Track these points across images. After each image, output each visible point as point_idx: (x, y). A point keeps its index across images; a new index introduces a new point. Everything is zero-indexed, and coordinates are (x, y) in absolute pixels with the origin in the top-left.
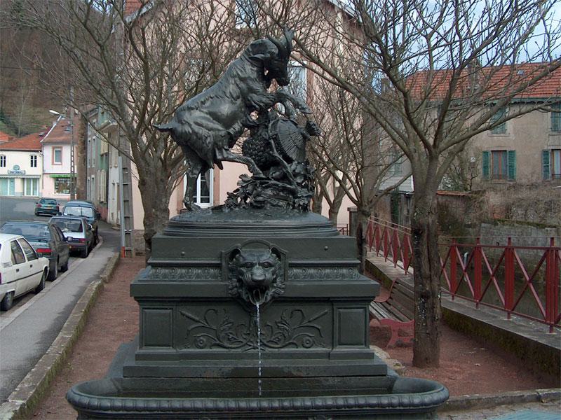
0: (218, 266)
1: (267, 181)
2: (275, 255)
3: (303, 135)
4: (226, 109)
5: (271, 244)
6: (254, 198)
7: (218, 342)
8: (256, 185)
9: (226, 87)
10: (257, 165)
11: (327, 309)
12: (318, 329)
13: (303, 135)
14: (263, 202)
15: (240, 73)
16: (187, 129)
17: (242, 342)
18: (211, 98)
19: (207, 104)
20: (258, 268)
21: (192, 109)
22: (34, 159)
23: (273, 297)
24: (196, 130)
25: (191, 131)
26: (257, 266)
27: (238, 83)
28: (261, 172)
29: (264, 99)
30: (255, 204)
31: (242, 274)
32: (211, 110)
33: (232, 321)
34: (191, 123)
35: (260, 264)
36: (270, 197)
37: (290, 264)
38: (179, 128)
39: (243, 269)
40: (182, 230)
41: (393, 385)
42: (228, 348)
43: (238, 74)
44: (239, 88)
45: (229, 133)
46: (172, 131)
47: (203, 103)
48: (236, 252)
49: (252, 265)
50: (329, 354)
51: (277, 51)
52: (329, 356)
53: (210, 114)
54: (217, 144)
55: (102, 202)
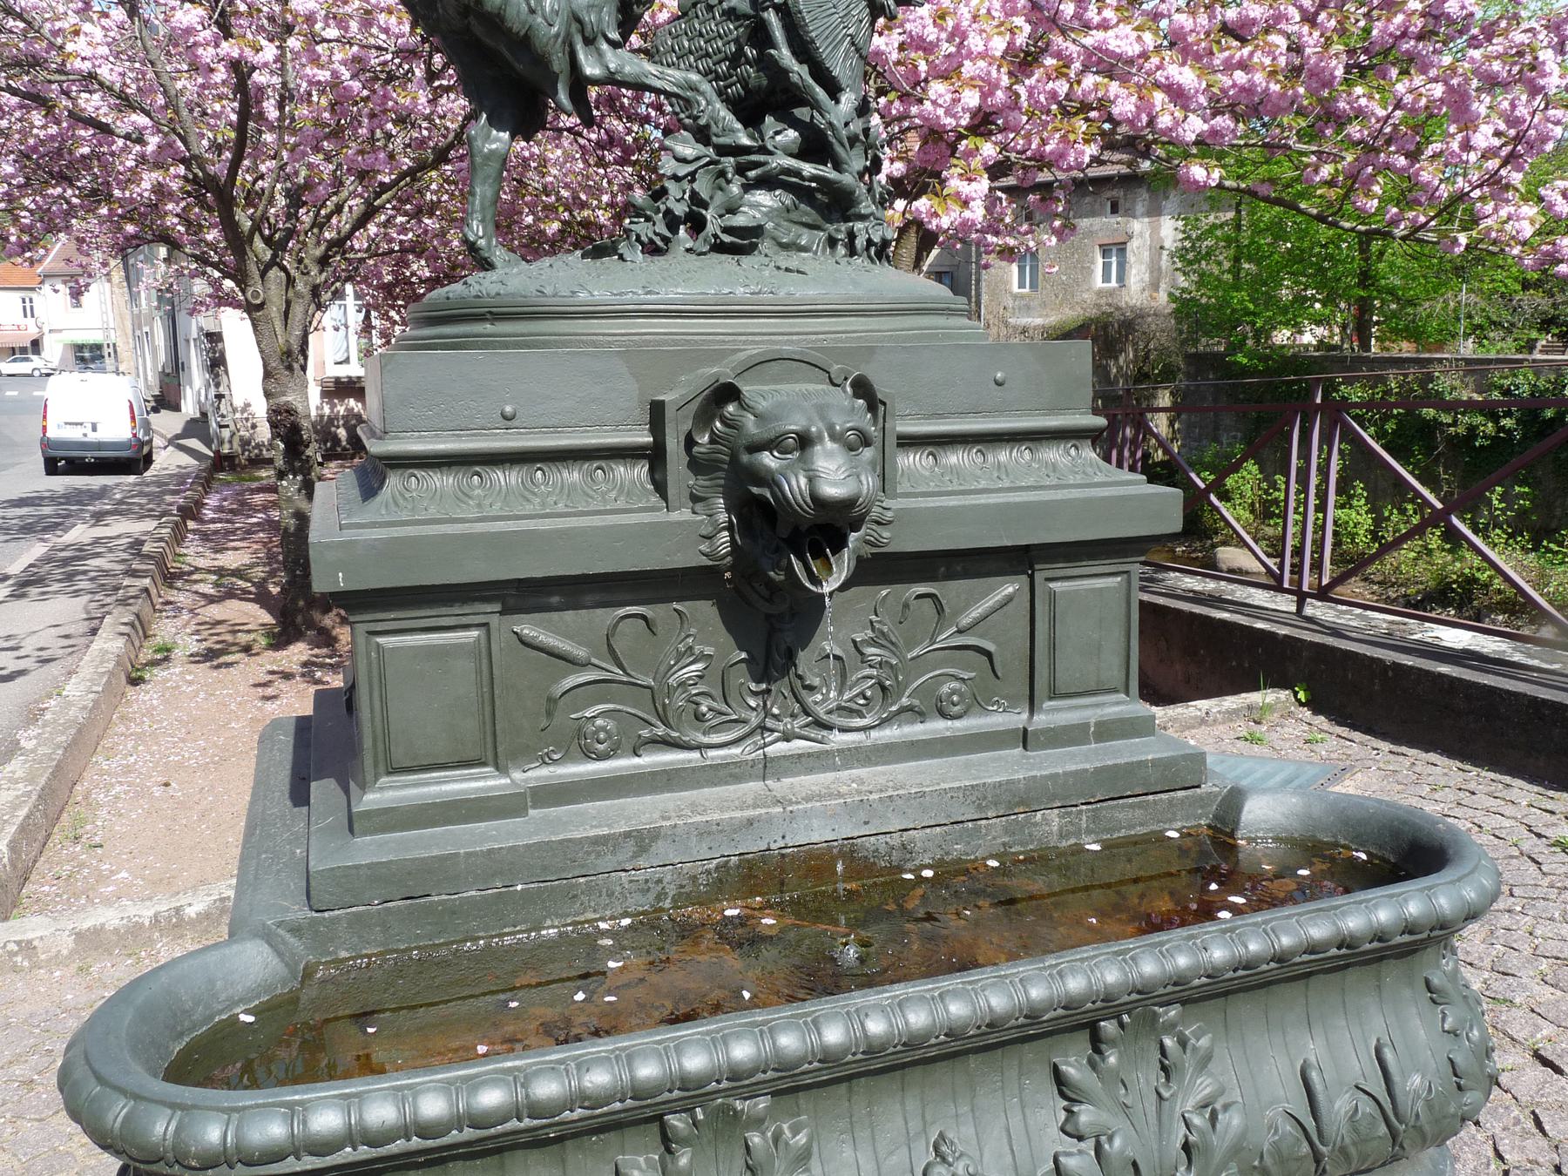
1: (762, 158)
7: (661, 731)
8: (722, 174)
11: (1009, 587)
12: (989, 655)
14: (757, 231)
17: (745, 722)
20: (829, 455)
22: (28, 304)
26: (829, 444)
28: (739, 126)
30: (727, 239)
33: (709, 651)
39: (769, 460)
40: (488, 327)
41: (1236, 822)
42: (699, 747)
48: (726, 393)
49: (805, 441)
50: (1025, 730)
52: (1025, 738)
54: (579, 20)
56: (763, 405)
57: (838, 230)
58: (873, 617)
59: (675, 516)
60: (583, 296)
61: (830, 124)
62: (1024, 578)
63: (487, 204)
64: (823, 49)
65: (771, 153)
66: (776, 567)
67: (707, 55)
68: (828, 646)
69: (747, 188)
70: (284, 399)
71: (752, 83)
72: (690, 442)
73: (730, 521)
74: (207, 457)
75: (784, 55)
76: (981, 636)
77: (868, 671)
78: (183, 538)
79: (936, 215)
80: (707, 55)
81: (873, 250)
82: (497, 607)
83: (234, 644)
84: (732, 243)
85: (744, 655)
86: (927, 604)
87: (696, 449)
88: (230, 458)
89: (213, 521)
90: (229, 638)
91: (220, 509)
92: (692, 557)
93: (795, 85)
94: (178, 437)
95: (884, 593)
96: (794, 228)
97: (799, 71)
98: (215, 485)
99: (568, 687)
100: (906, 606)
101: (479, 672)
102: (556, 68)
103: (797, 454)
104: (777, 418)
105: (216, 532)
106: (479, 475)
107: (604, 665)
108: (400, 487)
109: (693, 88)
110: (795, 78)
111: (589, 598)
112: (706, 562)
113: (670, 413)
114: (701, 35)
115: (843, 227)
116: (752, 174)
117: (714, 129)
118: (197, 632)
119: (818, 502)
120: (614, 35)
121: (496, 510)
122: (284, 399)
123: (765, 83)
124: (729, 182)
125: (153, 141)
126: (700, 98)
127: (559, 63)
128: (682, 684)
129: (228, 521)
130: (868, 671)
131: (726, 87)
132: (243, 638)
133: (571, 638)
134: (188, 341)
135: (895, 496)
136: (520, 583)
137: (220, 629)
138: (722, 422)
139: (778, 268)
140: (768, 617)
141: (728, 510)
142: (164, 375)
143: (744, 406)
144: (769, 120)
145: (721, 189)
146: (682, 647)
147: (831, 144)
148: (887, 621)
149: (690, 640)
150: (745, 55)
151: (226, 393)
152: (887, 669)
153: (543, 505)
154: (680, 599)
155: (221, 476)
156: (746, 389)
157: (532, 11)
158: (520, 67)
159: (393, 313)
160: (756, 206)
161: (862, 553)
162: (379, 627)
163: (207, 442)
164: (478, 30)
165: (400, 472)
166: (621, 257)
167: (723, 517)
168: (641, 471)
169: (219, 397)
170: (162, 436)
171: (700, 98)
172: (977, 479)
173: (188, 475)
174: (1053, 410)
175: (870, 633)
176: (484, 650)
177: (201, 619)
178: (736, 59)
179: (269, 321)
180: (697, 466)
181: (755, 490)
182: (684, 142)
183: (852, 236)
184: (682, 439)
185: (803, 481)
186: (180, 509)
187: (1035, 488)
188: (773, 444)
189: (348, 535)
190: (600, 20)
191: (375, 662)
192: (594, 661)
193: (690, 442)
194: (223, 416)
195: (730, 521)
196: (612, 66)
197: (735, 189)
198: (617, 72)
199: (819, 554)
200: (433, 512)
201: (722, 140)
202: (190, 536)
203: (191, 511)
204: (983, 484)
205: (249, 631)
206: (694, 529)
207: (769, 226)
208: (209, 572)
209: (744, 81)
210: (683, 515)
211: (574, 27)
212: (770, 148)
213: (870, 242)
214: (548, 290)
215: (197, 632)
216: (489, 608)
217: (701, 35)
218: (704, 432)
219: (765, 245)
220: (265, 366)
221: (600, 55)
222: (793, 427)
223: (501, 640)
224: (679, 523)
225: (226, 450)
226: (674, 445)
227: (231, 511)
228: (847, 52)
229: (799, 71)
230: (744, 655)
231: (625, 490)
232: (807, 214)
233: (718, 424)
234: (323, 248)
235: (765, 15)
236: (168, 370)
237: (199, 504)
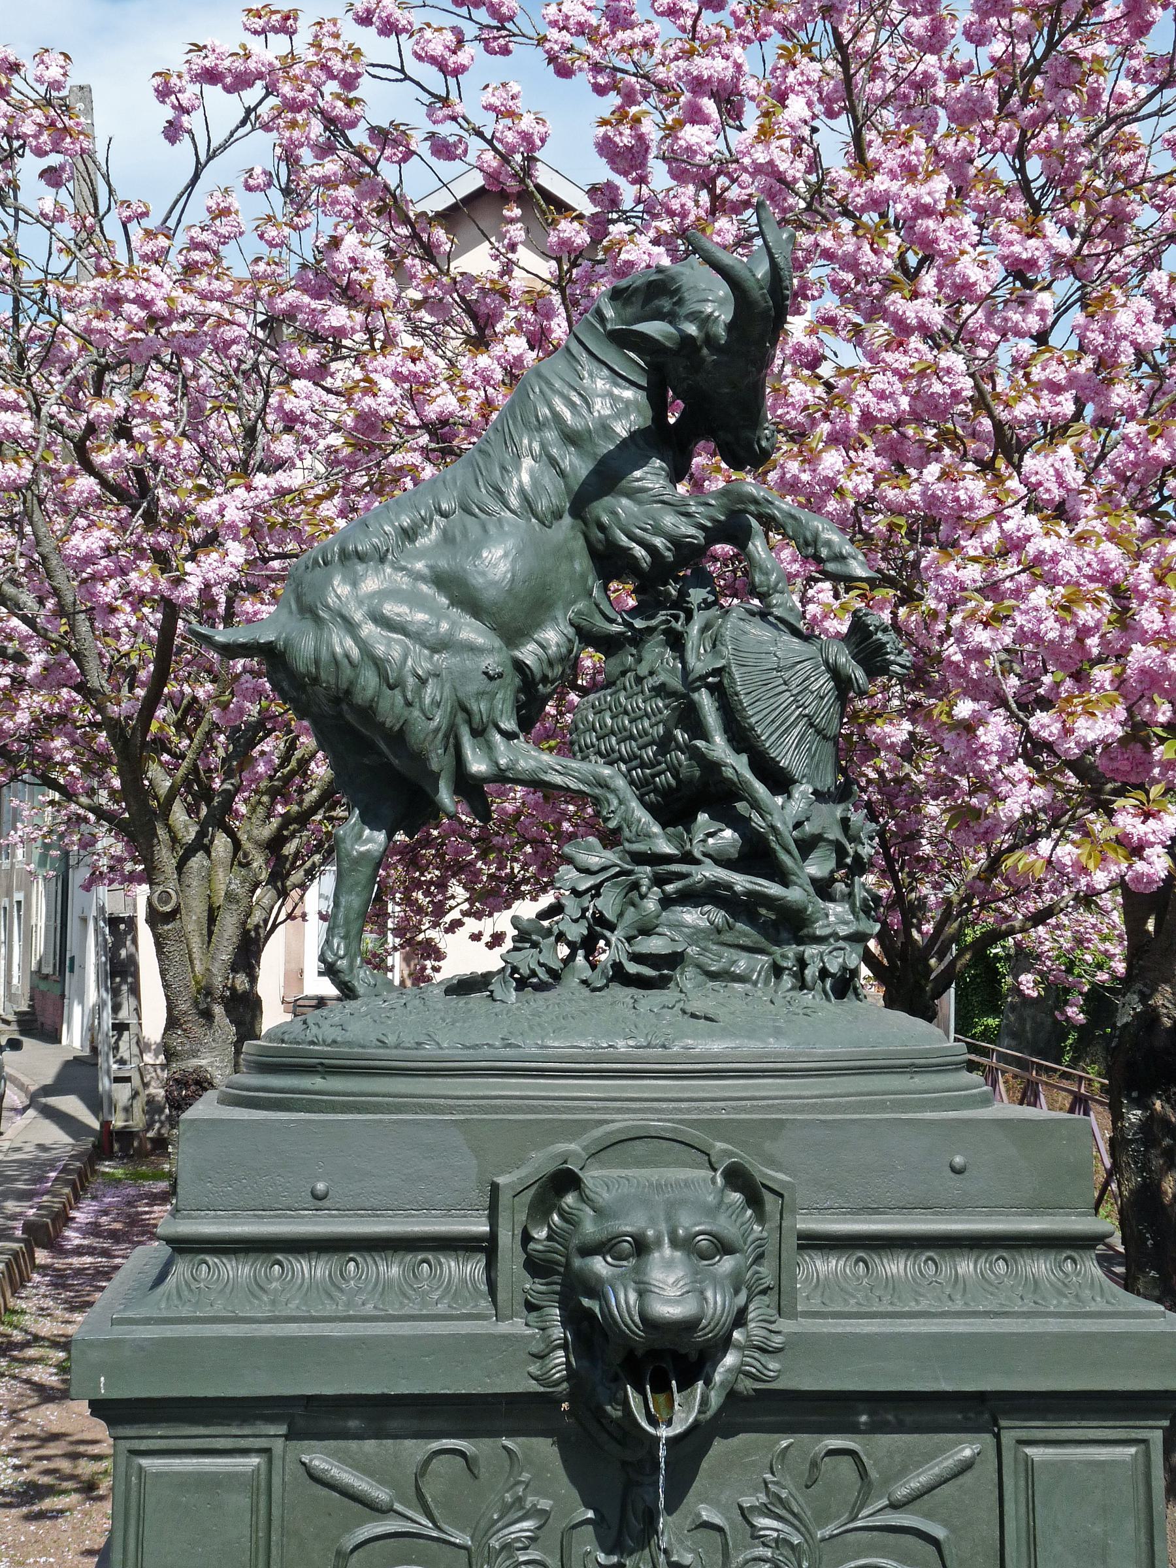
0: (486, 1246)
2: (737, 1196)
3: (835, 672)
4: (496, 563)
5: (720, 1145)
6: (629, 939)
8: (635, 886)
9: (503, 468)
10: (641, 799)
13: (835, 672)
14: (675, 960)
15: (567, 414)
16: (342, 644)
18: (444, 515)
19: (429, 539)
20: (669, 1265)
21: (361, 557)
23: (732, 1396)
24: (380, 650)
25: (355, 653)
26: (667, 1251)
27: (554, 451)
28: (656, 829)
29: (669, 520)
30: (632, 968)
31: (595, 1289)
32: (443, 564)
33: (545, 1504)
34: (358, 616)
35: (675, 1243)
36: (696, 936)
37: (802, 1236)
38: (306, 647)
39: (600, 1265)
40: (318, 1082)
43: (557, 416)
44: (562, 474)
45: (519, 666)
46: (272, 656)
47: (409, 534)
48: (564, 1181)
49: (641, 1247)
51: (725, 316)
53: (441, 581)
55: (46, 977)
56: (604, 1197)
57: (784, 957)
58: (768, 1476)
59: (504, 1327)
60: (429, 1049)
61: (773, 828)
62: (988, 1438)
63: (353, 916)
64: (765, 735)
65: (697, 862)
66: (612, 1400)
67: (631, 737)
68: (708, 1514)
69: (667, 902)
70: (194, 1062)
71: (684, 773)
72: (527, 1238)
73: (565, 1338)
74: (87, 1129)
75: (719, 747)
76: (928, 1516)
77: (761, 1551)
78: (24, 1280)
79: (1084, 870)
80: (631, 737)
81: (829, 982)
82: (282, 1429)
83: (72, 1477)
84: (638, 975)
85: (590, 1514)
86: (846, 1463)
87: (532, 1246)
88: (125, 1135)
89: (79, 1251)
90: (65, 1465)
91: (94, 1230)
92: (519, 1381)
93: (730, 780)
94: (47, 1091)
95: (784, 1444)
96: (728, 953)
97: (737, 765)
98: (96, 1183)
99: (362, 1538)
100: (814, 1465)
101: (254, 1510)
102: (435, 766)
103: (633, 1261)
104: (615, 1216)
105: (79, 1272)
106: (280, 1263)
107: (409, 1513)
108: (188, 1275)
109: (603, 784)
110: (728, 773)
111: (394, 1425)
112: (534, 1387)
113: (504, 1199)
114: (626, 712)
115: (791, 950)
116: (670, 888)
117: (626, 833)
118: (15, 1452)
119: (650, 1323)
120: (509, 725)
121: (291, 1309)
122: (194, 1062)
123: (698, 774)
124: (643, 897)
125: (38, 659)
126: (610, 796)
127: (439, 760)
128: (506, 1547)
129: (106, 1253)
130: (761, 1551)
131: (654, 776)
132: (86, 1468)
133: (371, 1475)
134: (84, 920)
135: (794, 1315)
136: (310, 1401)
137: (51, 1449)
138: (561, 1216)
139: (684, 1012)
140: (624, 1464)
141: (564, 1324)
142: (39, 975)
143: (584, 1199)
144: (703, 817)
145: (634, 905)
146: (508, 1497)
147: (774, 851)
148: (788, 1482)
149: (520, 1490)
150: (675, 739)
151: (133, 1021)
152: (786, 1551)
153: (348, 1304)
154: (511, 1434)
155: (106, 1167)
156: (591, 1177)
157: (409, 704)
158: (396, 762)
159: (419, 895)
160: (678, 926)
161: (740, 1387)
162: (143, 1445)
163: (95, 1103)
164: (350, 718)
165: (189, 1257)
166: (491, 996)
167: (558, 1332)
168: (473, 1268)
169: (120, 1028)
170: (22, 1087)
171: (610, 796)
172: (917, 1295)
173: (51, 1164)
174: (1035, 1208)
175: (763, 1498)
176: (263, 1484)
177: (26, 1429)
178: (665, 744)
179: (182, 937)
180: (536, 1267)
181: (586, 1302)
182: (589, 849)
183: (802, 963)
184: (518, 1231)
185: (633, 1297)
186: (28, 1227)
187: (997, 1314)
188: (603, 1247)
189: (119, 1332)
190: (491, 709)
191: (134, 1489)
192: (398, 1506)
193: (527, 1238)
194: (122, 1062)
195: (565, 1338)
196: (503, 762)
197: (651, 905)
198: (508, 769)
199: (661, 1387)
200: (219, 1309)
201: (636, 847)
202: (36, 1277)
203: (45, 1234)
204: (924, 1305)
205: (98, 1458)
206: (521, 1347)
207: (692, 950)
208: (55, 1344)
209: (675, 770)
210: (517, 1326)
211: (460, 717)
212: (697, 854)
213: (824, 973)
214: (391, 1040)
215: (15, 1452)
216: (272, 1430)
217: (626, 712)
218: (542, 1225)
219: (687, 978)
220: (170, 1008)
221: (490, 747)
222: (628, 1229)
223: (285, 1475)
224: (505, 1337)
225: (118, 1122)
226: (507, 1239)
227: (114, 1236)
228: (802, 737)
229: (737, 765)
230: (590, 1514)
231: (455, 1292)
232: (746, 935)
233: (556, 1217)
234: (275, 822)
235: (696, 696)
236: (47, 970)
237: (63, 1219)
